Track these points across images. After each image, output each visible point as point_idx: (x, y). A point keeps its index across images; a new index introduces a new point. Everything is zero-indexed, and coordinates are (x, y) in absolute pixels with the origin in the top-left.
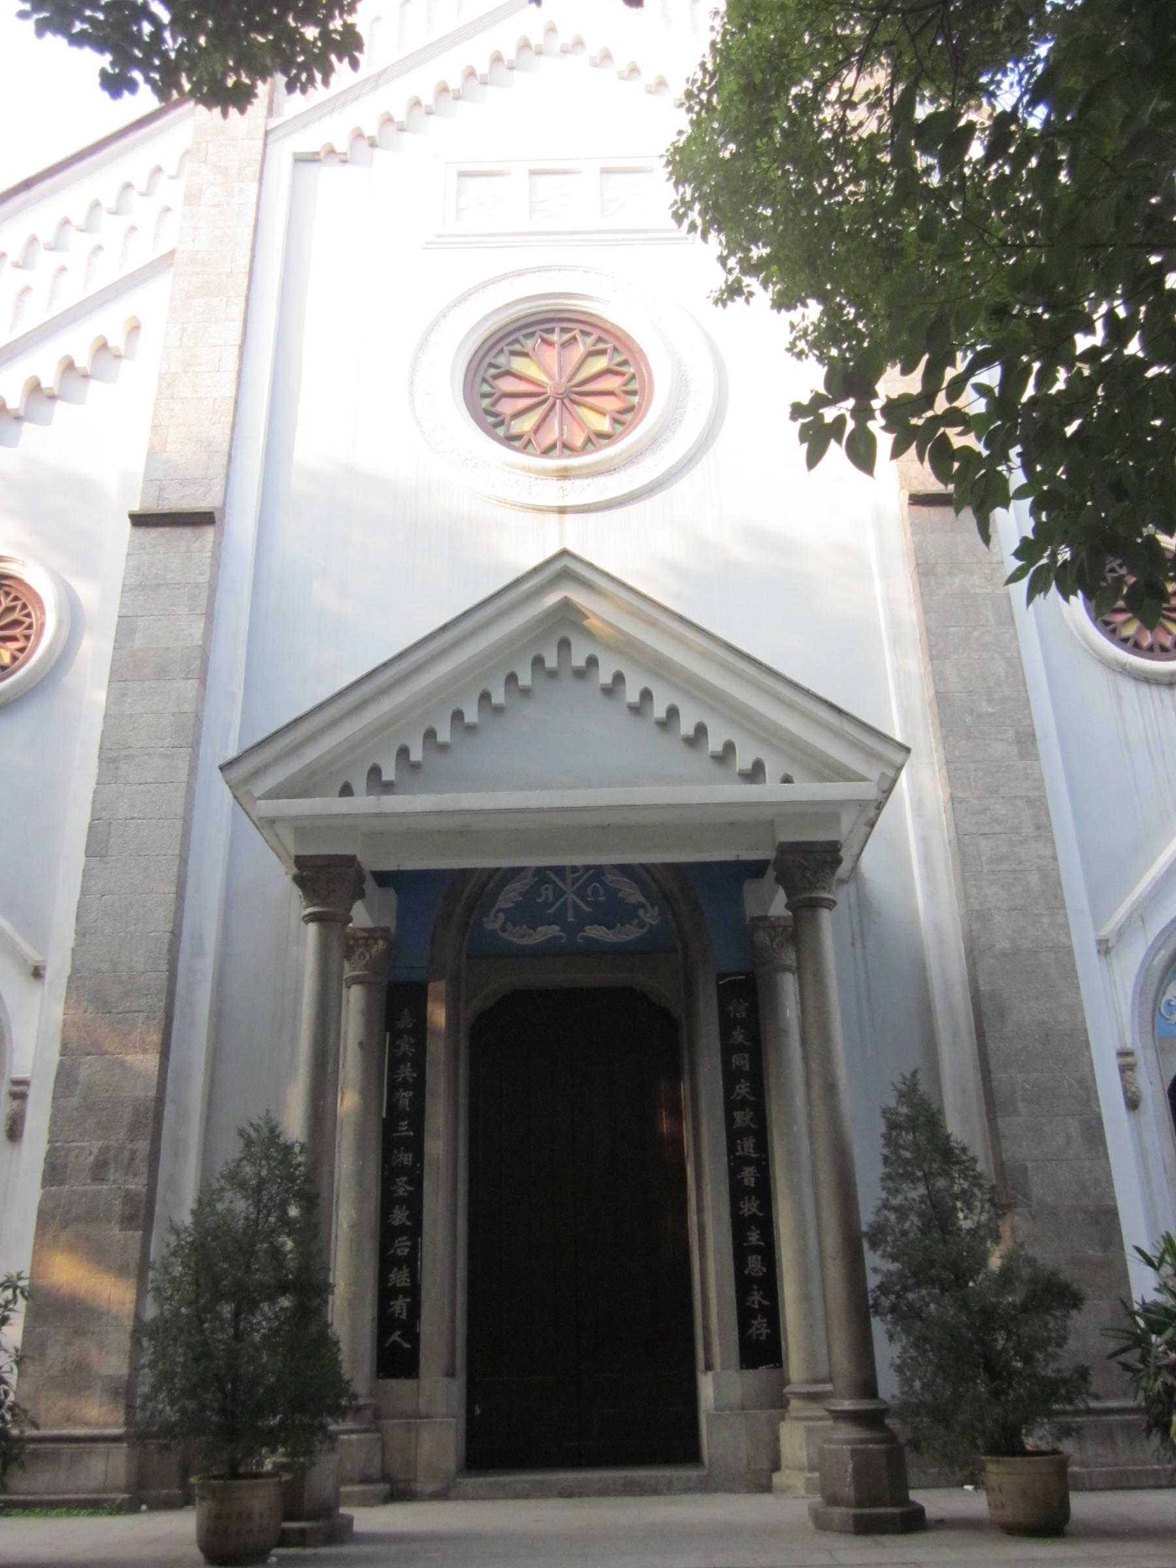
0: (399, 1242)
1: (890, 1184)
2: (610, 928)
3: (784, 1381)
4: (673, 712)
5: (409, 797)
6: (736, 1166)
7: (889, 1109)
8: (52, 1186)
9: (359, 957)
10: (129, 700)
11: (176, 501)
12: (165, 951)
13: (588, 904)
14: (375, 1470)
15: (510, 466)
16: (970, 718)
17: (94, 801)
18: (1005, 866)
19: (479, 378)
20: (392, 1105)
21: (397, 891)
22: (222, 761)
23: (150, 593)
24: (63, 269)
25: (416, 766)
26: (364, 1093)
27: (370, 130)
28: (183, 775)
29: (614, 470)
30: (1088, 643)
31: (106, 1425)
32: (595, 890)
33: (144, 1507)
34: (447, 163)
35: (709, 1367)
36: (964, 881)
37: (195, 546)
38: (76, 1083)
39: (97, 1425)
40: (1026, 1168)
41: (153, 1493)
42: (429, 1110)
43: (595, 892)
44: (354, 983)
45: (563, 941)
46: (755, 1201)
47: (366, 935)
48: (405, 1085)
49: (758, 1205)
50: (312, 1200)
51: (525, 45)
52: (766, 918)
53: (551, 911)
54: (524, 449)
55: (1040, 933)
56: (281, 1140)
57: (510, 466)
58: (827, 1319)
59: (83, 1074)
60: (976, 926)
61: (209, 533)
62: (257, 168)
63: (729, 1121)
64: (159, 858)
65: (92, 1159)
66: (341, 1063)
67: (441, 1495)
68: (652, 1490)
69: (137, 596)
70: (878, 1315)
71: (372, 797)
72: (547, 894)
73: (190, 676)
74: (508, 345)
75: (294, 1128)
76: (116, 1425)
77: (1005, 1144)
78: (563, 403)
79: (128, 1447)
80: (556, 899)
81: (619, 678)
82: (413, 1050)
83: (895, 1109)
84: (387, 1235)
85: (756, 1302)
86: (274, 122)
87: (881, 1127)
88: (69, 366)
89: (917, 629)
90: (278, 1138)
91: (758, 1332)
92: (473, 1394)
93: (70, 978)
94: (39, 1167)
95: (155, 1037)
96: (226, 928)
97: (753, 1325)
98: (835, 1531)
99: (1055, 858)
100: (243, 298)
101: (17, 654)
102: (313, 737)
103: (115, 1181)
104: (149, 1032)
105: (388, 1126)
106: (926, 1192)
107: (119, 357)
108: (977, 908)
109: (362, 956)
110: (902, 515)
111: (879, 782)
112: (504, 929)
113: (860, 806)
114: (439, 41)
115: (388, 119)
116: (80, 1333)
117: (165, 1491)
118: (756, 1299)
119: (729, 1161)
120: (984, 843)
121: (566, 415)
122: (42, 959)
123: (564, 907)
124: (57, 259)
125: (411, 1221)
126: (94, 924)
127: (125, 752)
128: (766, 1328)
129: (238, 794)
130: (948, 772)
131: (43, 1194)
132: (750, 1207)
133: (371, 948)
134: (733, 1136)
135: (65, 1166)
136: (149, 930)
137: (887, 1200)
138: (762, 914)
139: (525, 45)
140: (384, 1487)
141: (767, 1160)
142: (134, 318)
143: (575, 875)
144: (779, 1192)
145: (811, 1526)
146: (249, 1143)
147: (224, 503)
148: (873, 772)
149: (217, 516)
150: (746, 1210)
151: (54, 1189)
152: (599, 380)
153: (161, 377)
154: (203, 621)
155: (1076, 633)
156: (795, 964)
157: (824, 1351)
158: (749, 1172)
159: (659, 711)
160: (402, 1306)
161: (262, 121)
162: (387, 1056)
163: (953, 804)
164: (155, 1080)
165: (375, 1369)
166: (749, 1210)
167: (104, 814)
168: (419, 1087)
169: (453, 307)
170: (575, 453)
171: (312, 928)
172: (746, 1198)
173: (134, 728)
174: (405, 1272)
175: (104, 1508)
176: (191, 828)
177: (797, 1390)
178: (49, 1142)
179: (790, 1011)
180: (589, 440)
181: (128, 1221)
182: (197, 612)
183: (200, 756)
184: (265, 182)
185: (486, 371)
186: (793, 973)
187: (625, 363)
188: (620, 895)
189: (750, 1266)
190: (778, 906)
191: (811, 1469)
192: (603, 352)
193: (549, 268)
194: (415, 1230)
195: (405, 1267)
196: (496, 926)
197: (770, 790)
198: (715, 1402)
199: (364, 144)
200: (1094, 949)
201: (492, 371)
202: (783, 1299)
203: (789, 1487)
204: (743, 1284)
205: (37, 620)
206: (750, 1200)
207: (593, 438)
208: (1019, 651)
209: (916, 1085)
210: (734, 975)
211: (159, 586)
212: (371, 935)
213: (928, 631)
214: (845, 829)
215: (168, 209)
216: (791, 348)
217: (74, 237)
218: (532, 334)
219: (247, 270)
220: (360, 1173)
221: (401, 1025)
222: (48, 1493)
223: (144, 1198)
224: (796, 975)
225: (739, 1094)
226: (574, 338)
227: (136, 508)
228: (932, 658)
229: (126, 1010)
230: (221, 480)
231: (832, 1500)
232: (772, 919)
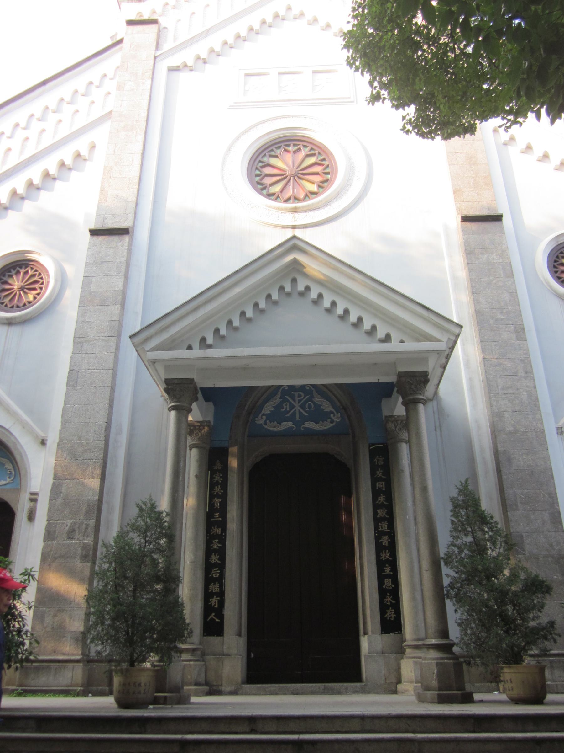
0: (214, 571)
1: (454, 534)
2: (316, 423)
3: (403, 640)
4: (346, 312)
5: (219, 350)
6: (378, 535)
7: (454, 498)
8: (48, 541)
9: (196, 435)
10: (88, 315)
11: (110, 224)
12: (103, 431)
13: (306, 411)
14: (202, 679)
15: (269, 207)
16: (492, 321)
17: (71, 362)
18: (510, 391)
19: (254, 168)
20: (211, 505)
21: (215, 404)
22: (130, 334)
23: (99, 265)
24: (60, 121)
25: (223, 337)
26: (198, 497)
27: (204, 55)
28: (113, 350)
29: (319, 208)
30: (551, 287)
31: (73, 655)
32: (310, 405)
33: (90, 695)
34: (240, 70)
35: (365, 633)
36: (490, 398)
37: (120, 244)
38: (61, 493)
39: (68, 655)
40: (522, 536)
41: (94, 688)
42: (229, 508)
43: (310, 406)
44: (193, 448)
45: (294, 429)
46: (388, 552)
47: (199, 424)
48: (218, 496)
49: (390, 555)
50: (171, 538)
51: (276, 16)
52: (392, 416)
53: (288, 415)
54: (276, 199)
55: (528, 423)
56: (158, 509)
57: (269, 207)
58: (423, 600)
59: (64, 489)
60: (496, 419)
61: (126, 238)
62: (151, 73)
63: (375, 513)
64: (101, 388)
65: (67, 528)
66: (186, 486)
67: (234, 693)
68: (339, 693)
69: (92, 267)
70: (449, 598)
71: (202, 350)
72: (286, 407)
73: (116, 304)
74: (268, 152)
75: (164, 505)
76: (78, 655)
77: (512, 524)
78: (294, 179)
79: (83, 665)
80: (291, 410)
81: (320, 296)
82: (222, 479)
83: (457, 498)
84: (208, 567)
85: (389, 602)
86: (159, 53)
87: (450, 506)
88: (62, 165)
89: (466, 281)
90: (155, 508)
91: (390, 616)
92: (250, 647)
93: (58, 443)
94: (43, 532)
95: (98, 471)
96: (132, 422)
97: (387, 612)
98: (428, 702)
99: (535, 387)
100: (143, 132)
101: (36, 296)
102: (174, 323)
103: (78, 539)
104: (95, 469)
105: (209, 515)
106: (472, 540)
107: (85, 160)
108: (496, 411)
109: (197, 435)
110: (458, 227)
111: (447, 343)
112: (265, 424)
113: (438, 354)
114: (237, 14)
115: (212, 51)
116: (61, 611)
117: (101, 688)
118: (389, 600)
119: (375, 533)
120: (499, 380)
121: (296, 184)
122: (45, 436)
123: (295, 413)
124: (57, 116)
125: (220, 561)
126: (70, 418)
127: (85, 339)
128: (394, 614)
129: (138, 349)
130: (481, 346)
131: (44, 545)
132: (385, 555)
133: (202, 431)
134: (377, 521)
135: (55, 531)
136: (96, 421)
137: (453, 542)
138: (391, 414)
139: (276, 16)
140: (206, 688)
141: (394, 533)
142: (93, 142)
143: (299, 398)
144: (400, 549)
145: (416, 701)
146: (141, 509)
147: (134, 225)
148: (444, 338)
149: (130, 230)
150: (384, 557)
151: (50, 542)
152: (311, 168)
153: (105, 168)
154: (123, 278)
155: (544, 282)
156: (407, 439)
157: (423, 625)
158: (385, 539)
159: (340, 311)
160: (215, 601)
161: (153, 52)
162: (209, 484)
163: (484, 361)
164: (98, 491)
165: (202, 631)
166: (385, 557)
167: (75, 367)
168: (224, 497)
169: (242, 135)
170: (300, 201)
171: (173, 413)
172: (384, 551)
173: (90, 328)
174: (217, 585)
175: (71, 694)
176: (116, 375)
177: (409, 644)
178: (47, 520)
179: (405, 461)
180: (307, 195)
181: (84, 558)
182: (120, 274)
183: (121, 341)
184: (154, 80)
185: (257, 164)
186: (406, 443)
187: (324, 160)
188: (322, 407)
189: (386, 584)
190: (400, 410)
191: (417, 682)
192: (313, 155)
193: (288, 117)
194: (222, 566)
195: (217, 583)
196: (262, 422)
197: (394, 346)
198: (368, 650)
199: (201, 62)
200: (555, 432)
201: (261, 164)
202: (402, 600)
203: (407, 691)
204: (382, 593)
205: (46, 280)
206: (385, 553)
207: (309, 194)
208: (516, 290)
209: (467, 486)
210: (378, 444)
211: (102, 262)
212: (202, 424)
213: (471, 280)
214: (431, 366)
215: (109, 93)
216: (403, 129)
217: (65, 107)
218: (279, 147)
219: (145, 119)
220: (196, 537)
221: (216, 468)
222: (44, 687)
223: (92, 547)
224: (408, 444)
225: (379, 501)
226: (300, 149)
227: (93, 227)
228: (473, 293)
229: (85, 458)
230: (132, 214)
231: (427, 688)
232: (396, 417)
